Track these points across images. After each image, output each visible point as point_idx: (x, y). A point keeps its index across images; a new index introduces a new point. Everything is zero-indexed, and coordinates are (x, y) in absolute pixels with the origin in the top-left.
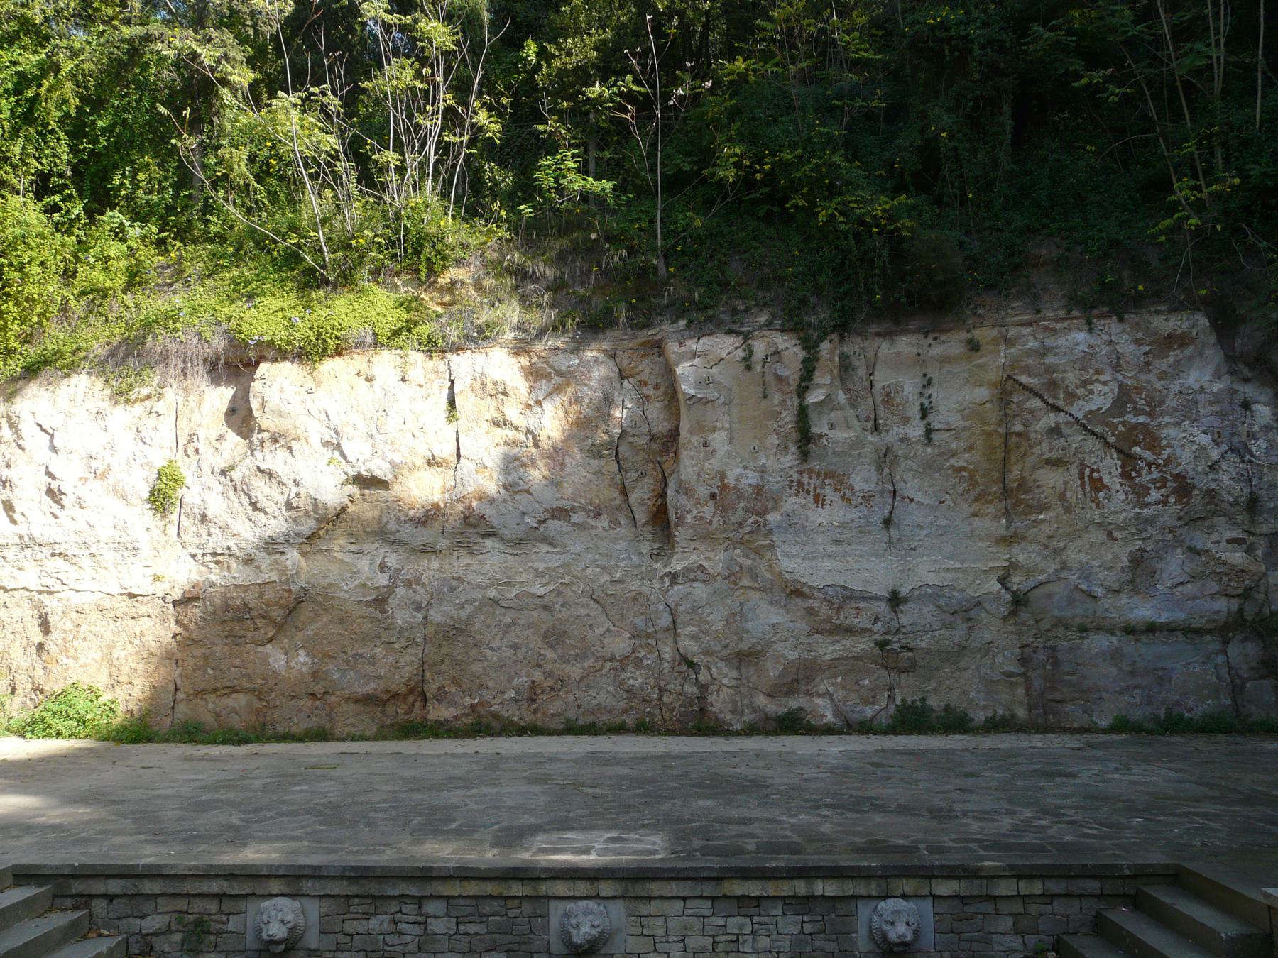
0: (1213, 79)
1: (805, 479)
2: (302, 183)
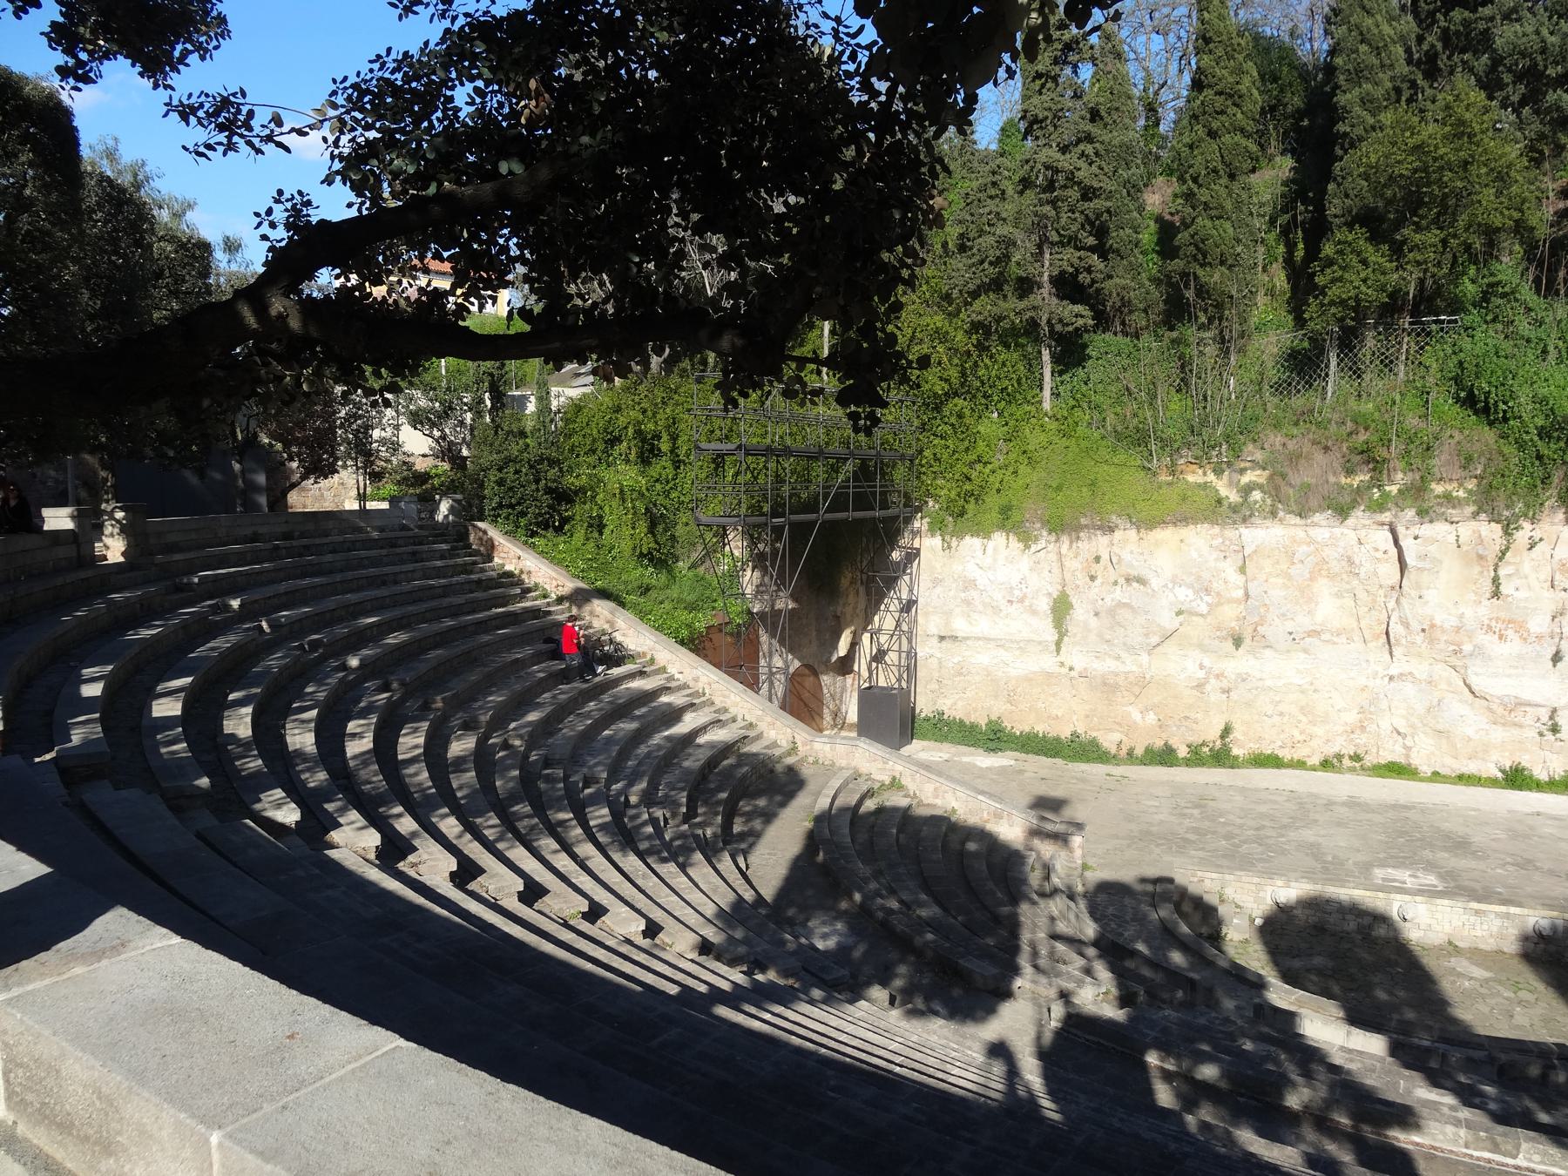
0: (1467, 1147)
1: (1493, 624)
2: (1052, 280)
